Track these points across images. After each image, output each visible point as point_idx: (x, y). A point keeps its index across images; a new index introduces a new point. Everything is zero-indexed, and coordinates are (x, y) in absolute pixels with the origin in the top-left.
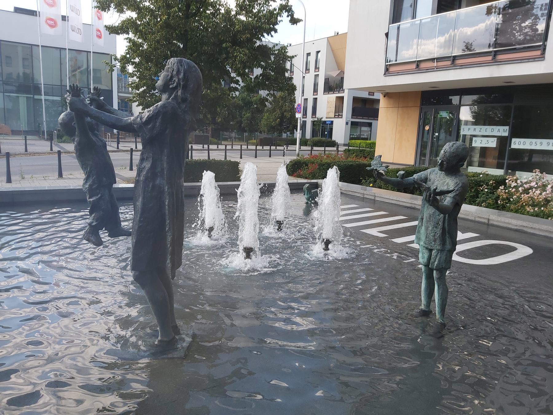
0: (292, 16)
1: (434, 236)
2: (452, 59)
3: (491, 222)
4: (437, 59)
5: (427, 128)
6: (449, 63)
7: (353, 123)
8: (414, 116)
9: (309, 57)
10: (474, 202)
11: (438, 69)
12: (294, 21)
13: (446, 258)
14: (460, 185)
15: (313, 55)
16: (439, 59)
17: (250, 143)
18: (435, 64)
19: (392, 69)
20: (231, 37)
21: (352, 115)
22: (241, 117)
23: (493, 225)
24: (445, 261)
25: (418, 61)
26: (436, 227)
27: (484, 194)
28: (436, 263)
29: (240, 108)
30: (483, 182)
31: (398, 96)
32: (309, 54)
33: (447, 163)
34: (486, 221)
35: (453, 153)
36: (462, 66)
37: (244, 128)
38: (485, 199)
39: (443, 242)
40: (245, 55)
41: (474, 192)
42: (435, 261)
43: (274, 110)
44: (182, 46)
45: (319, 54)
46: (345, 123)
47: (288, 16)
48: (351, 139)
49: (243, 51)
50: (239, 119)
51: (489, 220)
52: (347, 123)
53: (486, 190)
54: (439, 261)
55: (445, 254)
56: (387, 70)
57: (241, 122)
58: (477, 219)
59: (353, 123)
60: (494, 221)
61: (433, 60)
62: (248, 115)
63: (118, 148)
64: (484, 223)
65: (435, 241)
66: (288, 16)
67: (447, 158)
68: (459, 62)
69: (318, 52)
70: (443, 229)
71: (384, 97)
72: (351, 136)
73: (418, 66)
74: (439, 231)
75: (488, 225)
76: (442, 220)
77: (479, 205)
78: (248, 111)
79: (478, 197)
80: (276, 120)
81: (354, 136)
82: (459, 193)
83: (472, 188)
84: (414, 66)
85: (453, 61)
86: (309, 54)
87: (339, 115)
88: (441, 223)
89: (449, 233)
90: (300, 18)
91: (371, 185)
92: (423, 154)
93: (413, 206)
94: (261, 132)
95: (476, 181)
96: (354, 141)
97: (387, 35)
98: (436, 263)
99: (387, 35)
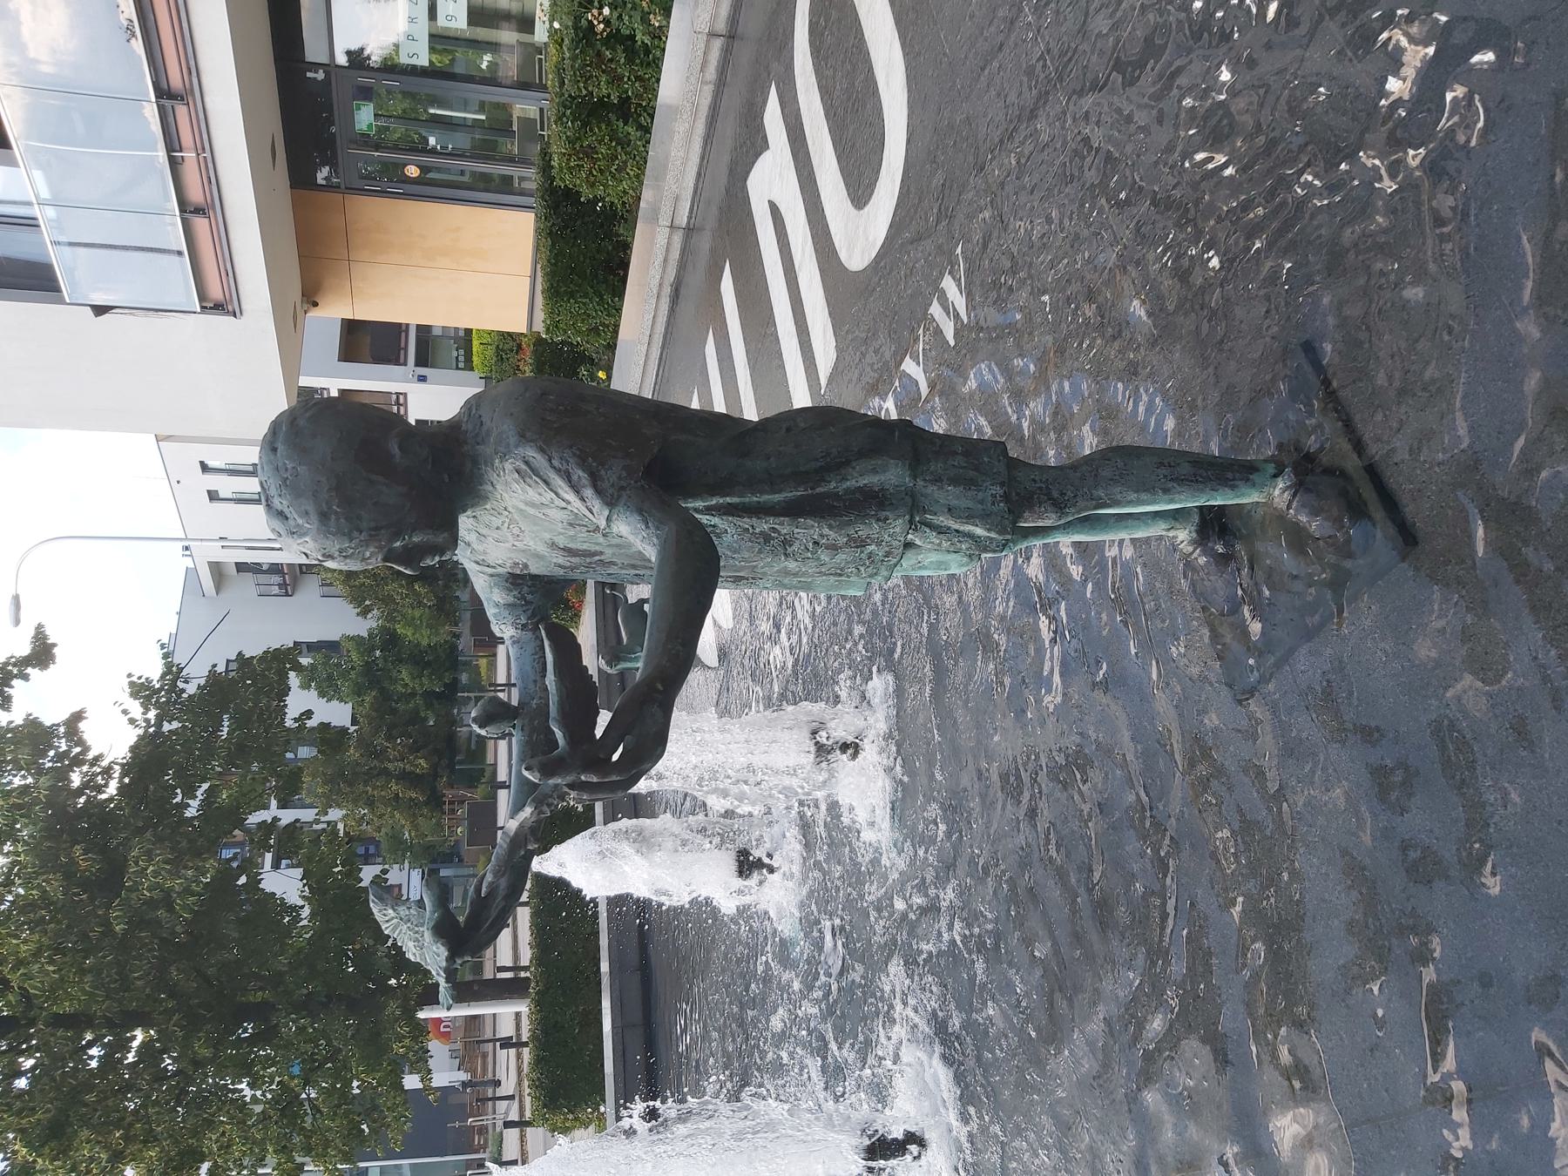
0: (26, 662)
1: (834, 548)
2: (167, 103)
3: (721, 26)
4: (170, 148)
5: (413, 171)
6: (181, 111)
7: (422, 361)
8: (373, 211)
9: (222, 495)
10: (647, 51)
11: (205, 146)
12: (42, 654)
13: (954, 481)
14: (531, 453)
15: (214, 482)
16: (172, 144)
17: (489, 677)
18: (189, 155)
19: (215, 292)
20: (92, 899)
21: (397, 363)
22: (413, 694)
23: (734, 19)
24: (969, 483)
25: (182, 210)
26: (786, 543)
27: (620, 17)
28: (979, 531)
29: (385, 697)
30: (577, 19)
31: (310, 262)
32: (213, 496)
33: (397, 535)
34: (717, 44)
35: (324, 517)
36: (192, 67)
37: (445, 685)
38: (637, 16)
39: (872, 503)
40: (149, 855)
41: (614, 49)
42: (970, 535)
43: (387, 600)
44: (139, 1036)
45: (211, 463)
46: (422, 385)
47: (26, 677)
48: (469, 366)
49: (137, 864)
50: (419, 700)
51: (712, 34)
52: (422, 379)
53: (606, 11)
54: (970, 517)
55: (932, 489)
56: (219, 308)
57: (429, 696)
58: (711, 73)
59: (422, 361)
60: (714, 17)
61: (175, 164)
62: (405, 674)
63: (511, 1098)
64: (727, 53)
65: (861, 544)
66: (26, 677)
67: (366, 544)
68: (176, 80)
69: (205, 468)
70: (793, 510)
71: (316, 304)
72: (461, 365)
73: (199, 211)
74: (808, 531)
75: (731, 36)
76: (746, 522)
77: (660, 35)
78: (394, 674)
79: (632, 37)
80: (418, 594)
81: (461, 358)
82: (583, 463)
83: (599, 54)
84: (200, 224)
85: (174, 95)
86: (213, 496)
87: (398, 403)
88: (763, 525)
89: (821, 474)
90: (32, 633)
91: (602, 375)
92: (505, 185)
93: (667, 290)
94: (457, 636)
95: (576, 42)
96: (475, 358)
97: (100, 310)
98: (979, 531)
99: (100, 310)
